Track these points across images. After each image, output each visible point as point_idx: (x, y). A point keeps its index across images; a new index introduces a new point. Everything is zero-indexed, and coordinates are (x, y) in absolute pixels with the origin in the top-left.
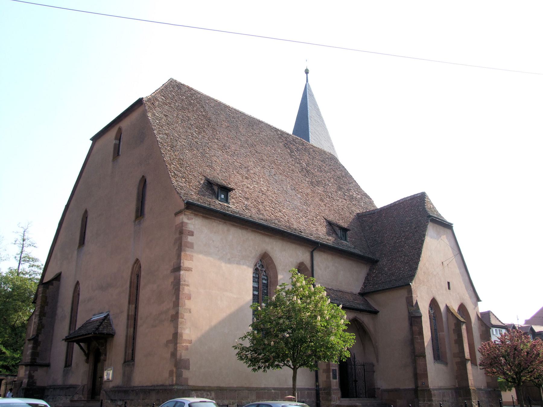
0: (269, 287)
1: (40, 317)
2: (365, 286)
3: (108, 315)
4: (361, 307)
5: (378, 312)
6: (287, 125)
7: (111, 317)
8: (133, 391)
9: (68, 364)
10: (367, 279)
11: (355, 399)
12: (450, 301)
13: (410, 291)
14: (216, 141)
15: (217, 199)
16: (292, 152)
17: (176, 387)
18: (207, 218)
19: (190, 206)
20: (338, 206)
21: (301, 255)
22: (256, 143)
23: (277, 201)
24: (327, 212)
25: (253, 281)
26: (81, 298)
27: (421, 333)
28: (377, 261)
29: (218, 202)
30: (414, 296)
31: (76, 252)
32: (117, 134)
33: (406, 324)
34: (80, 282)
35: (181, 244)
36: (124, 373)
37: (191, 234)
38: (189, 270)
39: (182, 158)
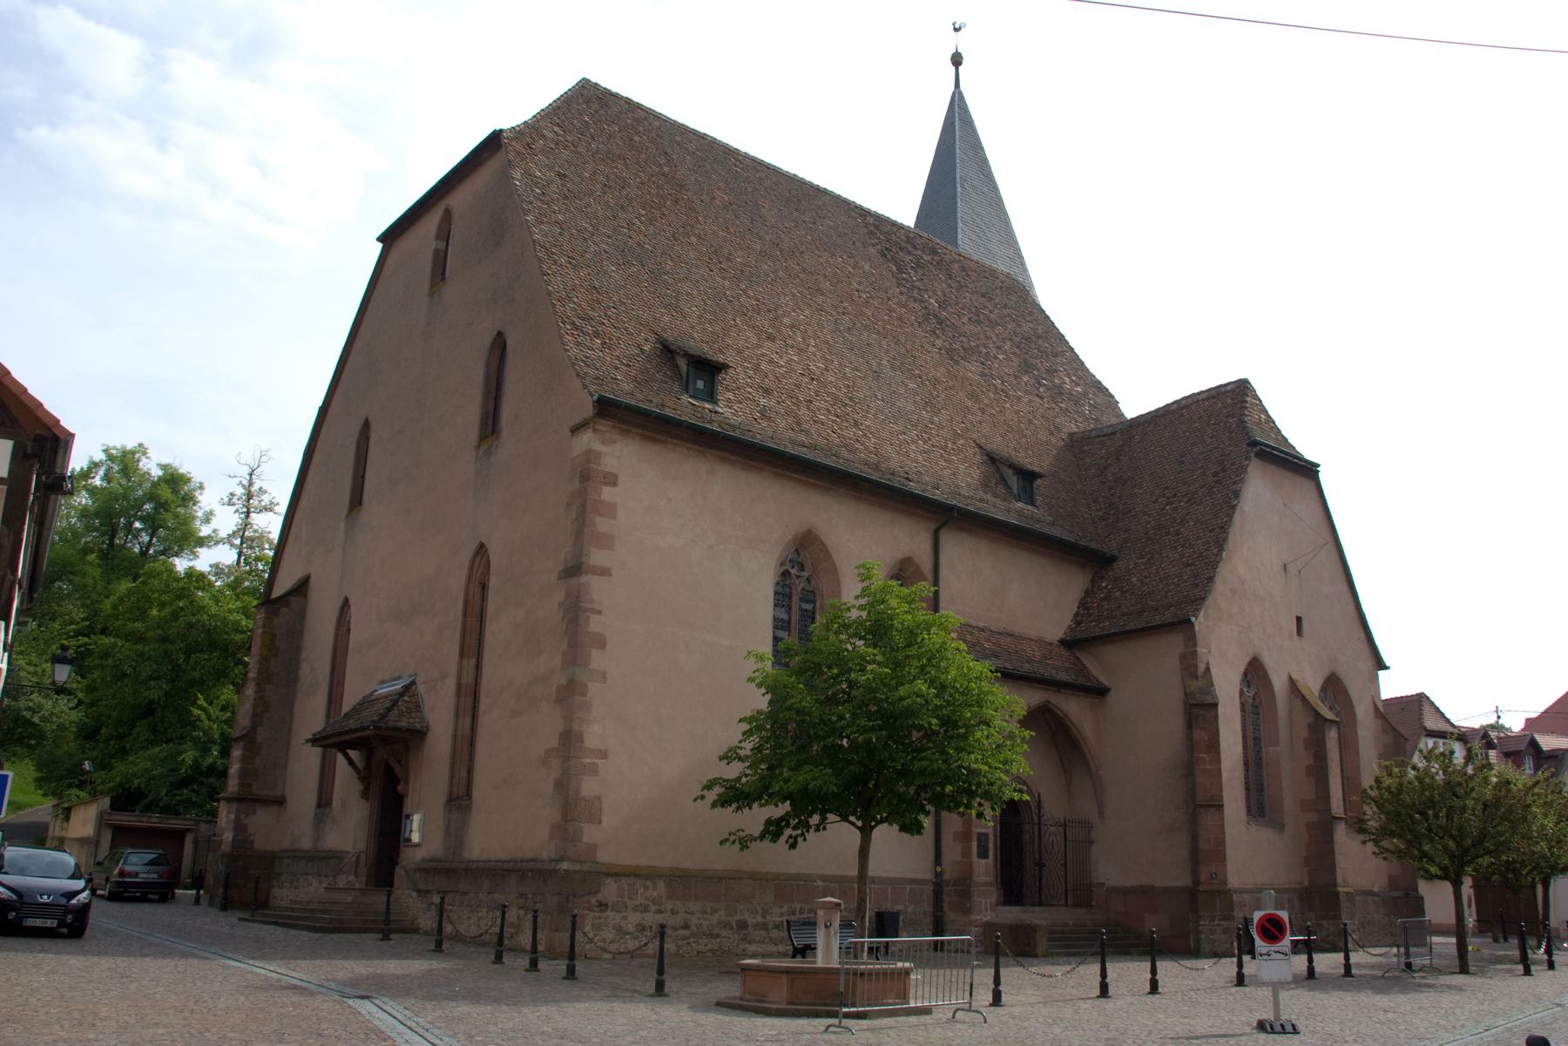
1: (258, 685)
2: (1078, 623)
3: (413, 683)
4: (1063, 676)
5: (1108, 690)
6: (898, 197)
7: (421, 688)
8: (466, 870)
9: (324, 801)
10: (1083, 604)
11: (1037, 909)
12: (1297, 667)
13: (1191, 638)
14: (694, 239)
15: (687, 390)
16: (900, 271)
17: (565, 866)
18: (655, 440)
19: (607, 409)
20: (1017, 412)
21: (905, 538)
22: (803, 248)
23: (851, 399)
24: (986, 429)
25: (776, 605)
26: (354, 639)
27: (1214, 746)
29: (685, 398)
30: (1201, 650)
31: (342, 525)
32: (440, 228)
33: (1177, 722)
34: (351, 602)
35: (583, 506)
36: (448, 827)
37: (612, 480)
38: (605, 572)
39: (597, 284)
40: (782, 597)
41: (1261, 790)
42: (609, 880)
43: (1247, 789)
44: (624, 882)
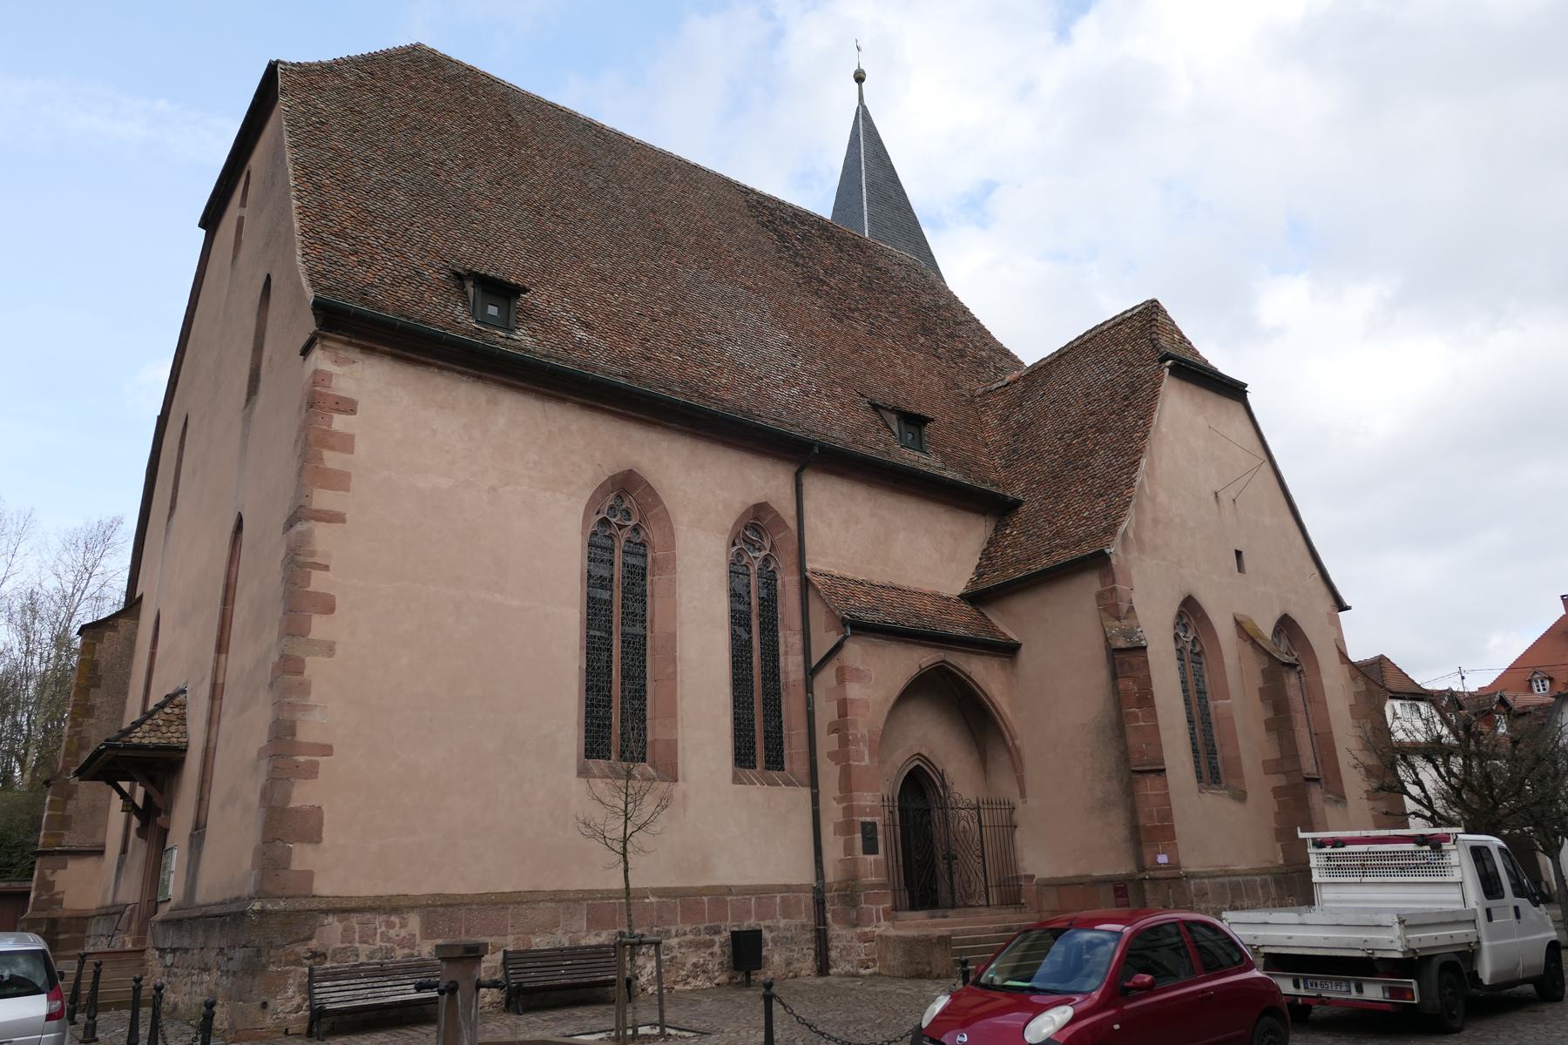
0: (649, 578)
2: (980, 576)
10: (986, 555)
11: (950, 912)
27: (1146, 699)
28: (1017, 504)
30: (1121, 587)
37: (348, 407)
38: (334, 518)
40: (598, 549)
41: (1212, 753)
42: (330, 919)
43: (1195, 751)
44: (354, 920)
